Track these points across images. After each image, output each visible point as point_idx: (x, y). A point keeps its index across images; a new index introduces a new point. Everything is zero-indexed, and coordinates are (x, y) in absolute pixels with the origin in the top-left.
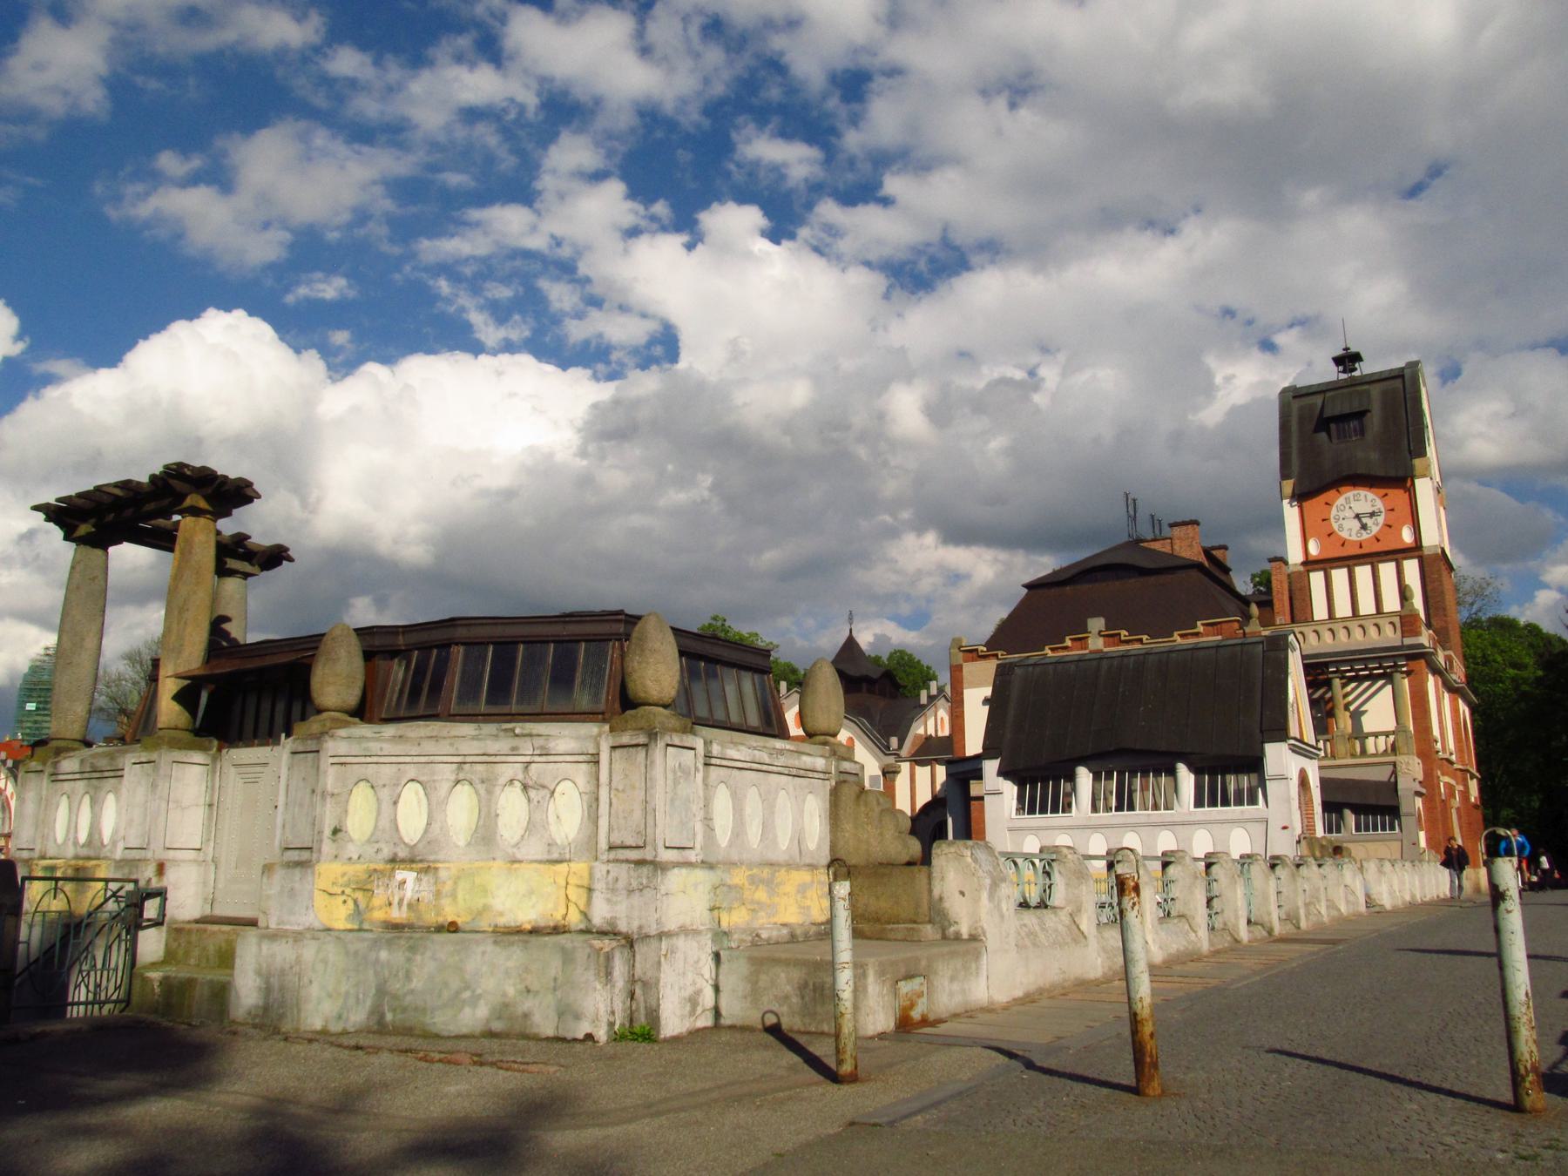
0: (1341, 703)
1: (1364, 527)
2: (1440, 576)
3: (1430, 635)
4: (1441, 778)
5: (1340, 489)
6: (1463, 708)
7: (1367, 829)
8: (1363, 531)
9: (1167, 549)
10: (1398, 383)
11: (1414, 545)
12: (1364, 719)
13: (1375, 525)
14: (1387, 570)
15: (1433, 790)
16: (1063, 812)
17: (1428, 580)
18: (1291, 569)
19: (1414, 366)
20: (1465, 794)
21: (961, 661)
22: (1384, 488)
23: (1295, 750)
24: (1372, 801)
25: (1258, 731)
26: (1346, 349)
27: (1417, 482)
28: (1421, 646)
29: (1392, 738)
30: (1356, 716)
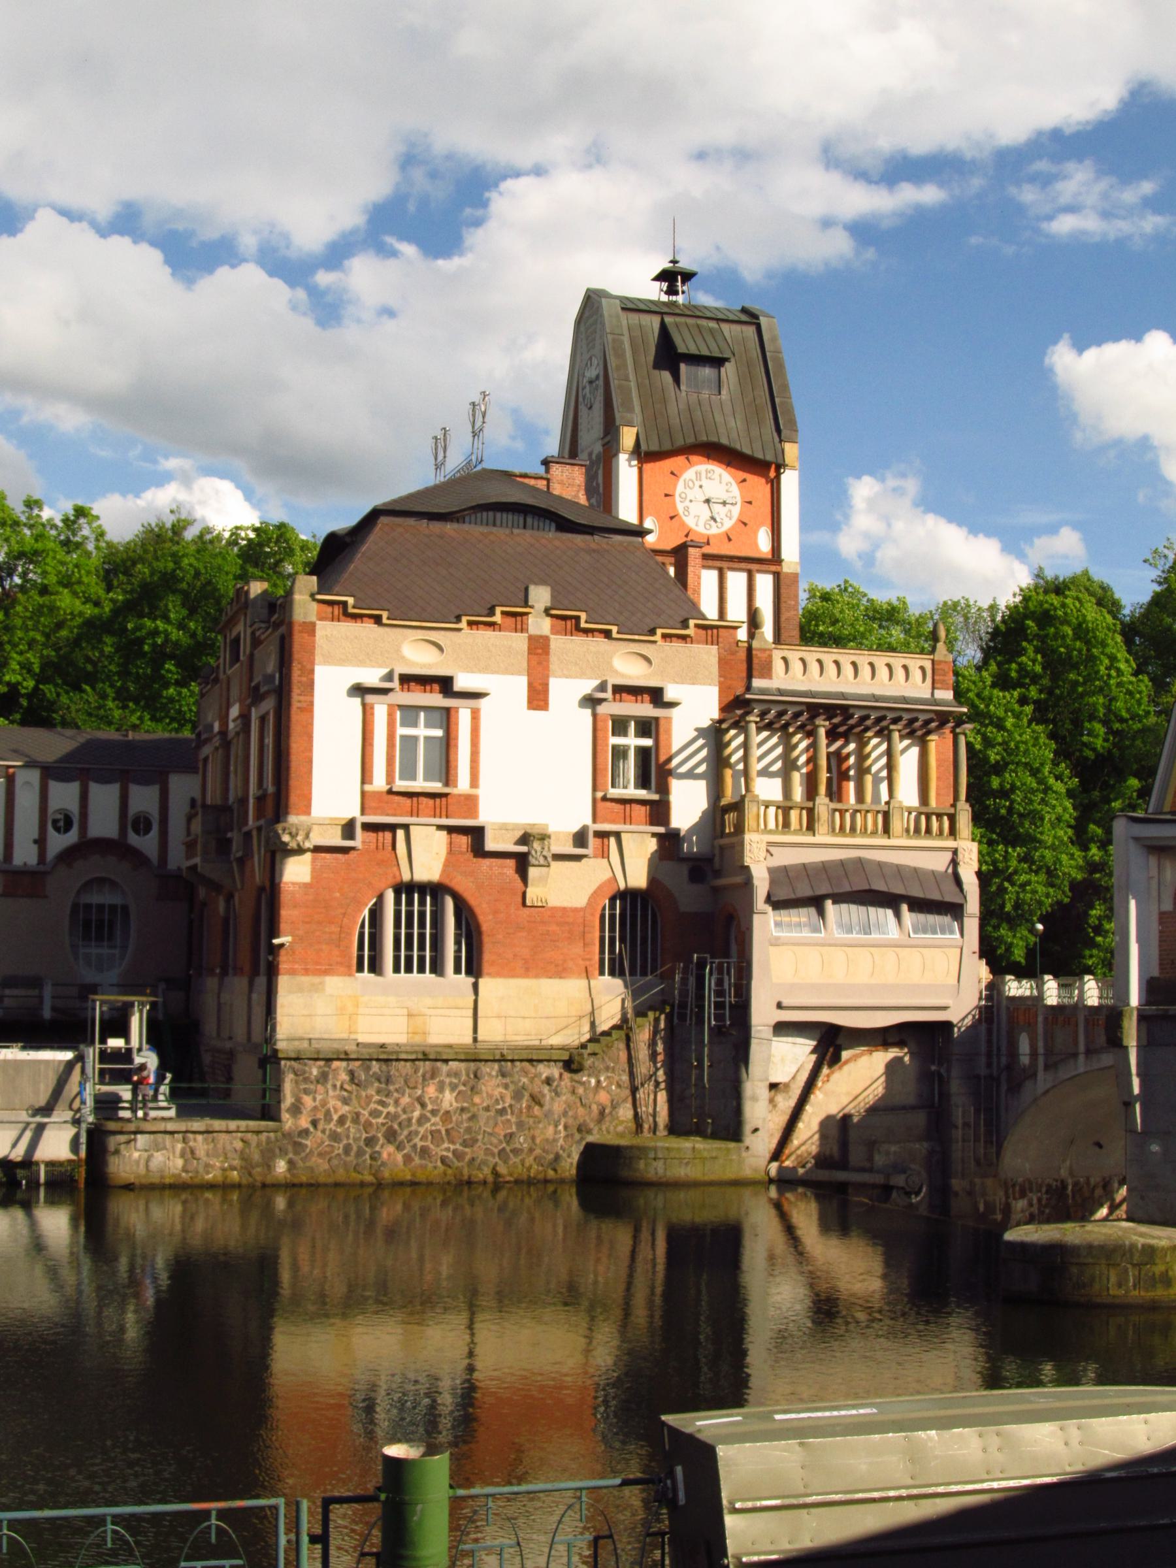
7: (409, 969)
11: (770, 556)
13: (728, 519)
21: (313, 618)
22: (744, 471)
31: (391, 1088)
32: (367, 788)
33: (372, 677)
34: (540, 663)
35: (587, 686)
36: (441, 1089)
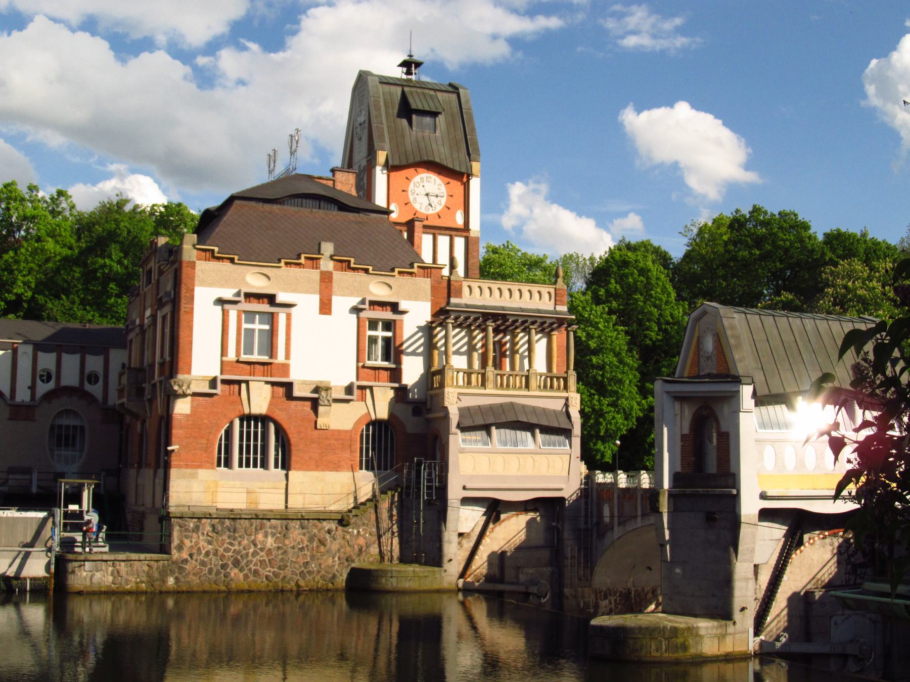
7: (248, 466)
11: (463, 227)
13: (439, 205)
14: (443, 241)
31: (237, 535)
32: (225, 359)
33: (228, 294)
34: (326, 287)
35: (354, 301)
36: (266, 536)
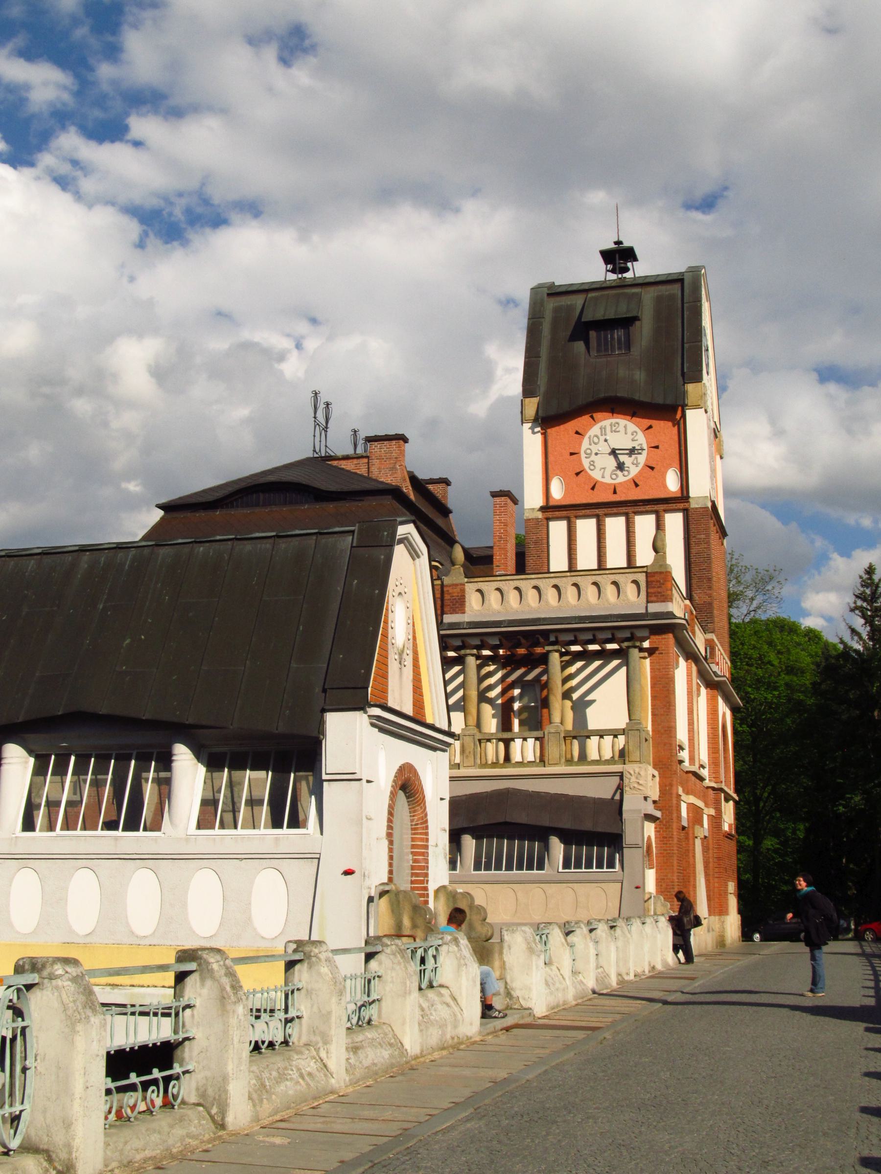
0: (558, 689)
1: (621, 467)
2: (708, 536)
3: (686, 606)
4: (684, 797)
5: (595, 415)
6: (724, 710)
7: (578, 865)
8: (619, 472)
9: (363, 471)
10: (676, 289)
11: (679, 495)
12: (589, 711)
13: (634, 467)
15: (671, 813)
16: (84, 828)
17: (693, 540)
18: (527, 515)
19: (695, 273)
20: (716, 820)
23: (382, 726)
24: (587, 826)
25: (318, 690)
26: (618, 243)
27: (689, 413)
28: (670, 615)
29: (621, 739)
30: (581, 707)
